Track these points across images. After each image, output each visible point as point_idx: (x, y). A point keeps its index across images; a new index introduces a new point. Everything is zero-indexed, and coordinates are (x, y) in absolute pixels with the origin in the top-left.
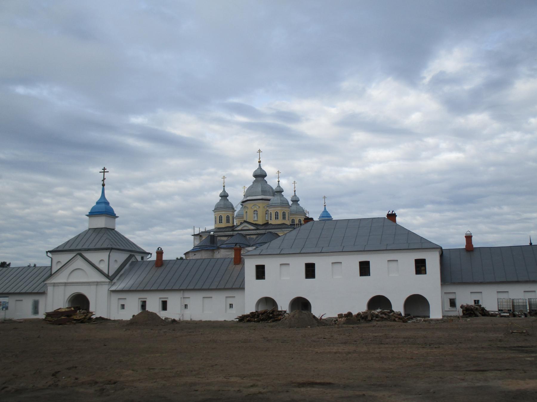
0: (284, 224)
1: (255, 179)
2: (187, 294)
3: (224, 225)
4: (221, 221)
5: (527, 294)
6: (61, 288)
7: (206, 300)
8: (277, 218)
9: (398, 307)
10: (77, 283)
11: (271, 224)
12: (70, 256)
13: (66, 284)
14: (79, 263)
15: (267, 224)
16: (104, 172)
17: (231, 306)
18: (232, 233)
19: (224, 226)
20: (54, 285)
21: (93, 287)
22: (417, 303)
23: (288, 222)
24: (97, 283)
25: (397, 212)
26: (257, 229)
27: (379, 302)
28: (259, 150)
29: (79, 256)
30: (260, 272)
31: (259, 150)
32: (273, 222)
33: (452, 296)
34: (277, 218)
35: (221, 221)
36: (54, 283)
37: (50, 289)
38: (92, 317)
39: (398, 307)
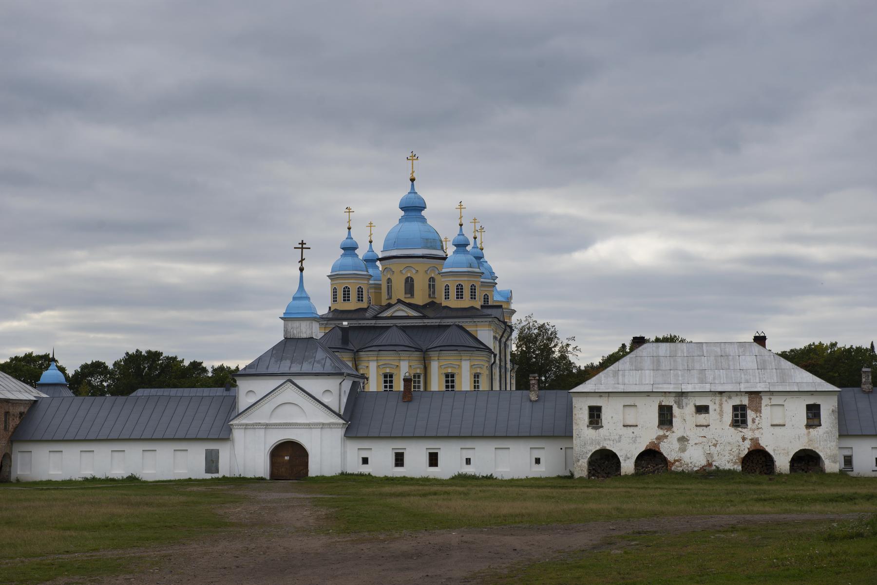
0: (472, 308)
1: (403, 213)
2: (469, 444)
3: (353, 305)
4: (346, 297)
5: (464, 451)
6: (261, 432)
7: (147, 454)
8: (460, 295)
9: (782, 463)
10: (280, 424)
11: (446, 307)
13: (267, 426)
14: (289, 394)
15: (432, 305)
16: (302, 248)
17: (538, 461)
18: (374, 322)
19: (353, 308)
20: (246, 426)
21: (316, 432)
22: (806, 460)
23: (478, 304)
24: (323, 426)
27: (758, 459)
29: (289, 384)
32: (453, 303)
33: (847, 453)
34: (460, 295)
35: (346, 297)
36: (247, 425)
37: (237, 434)
39: (782, 463)
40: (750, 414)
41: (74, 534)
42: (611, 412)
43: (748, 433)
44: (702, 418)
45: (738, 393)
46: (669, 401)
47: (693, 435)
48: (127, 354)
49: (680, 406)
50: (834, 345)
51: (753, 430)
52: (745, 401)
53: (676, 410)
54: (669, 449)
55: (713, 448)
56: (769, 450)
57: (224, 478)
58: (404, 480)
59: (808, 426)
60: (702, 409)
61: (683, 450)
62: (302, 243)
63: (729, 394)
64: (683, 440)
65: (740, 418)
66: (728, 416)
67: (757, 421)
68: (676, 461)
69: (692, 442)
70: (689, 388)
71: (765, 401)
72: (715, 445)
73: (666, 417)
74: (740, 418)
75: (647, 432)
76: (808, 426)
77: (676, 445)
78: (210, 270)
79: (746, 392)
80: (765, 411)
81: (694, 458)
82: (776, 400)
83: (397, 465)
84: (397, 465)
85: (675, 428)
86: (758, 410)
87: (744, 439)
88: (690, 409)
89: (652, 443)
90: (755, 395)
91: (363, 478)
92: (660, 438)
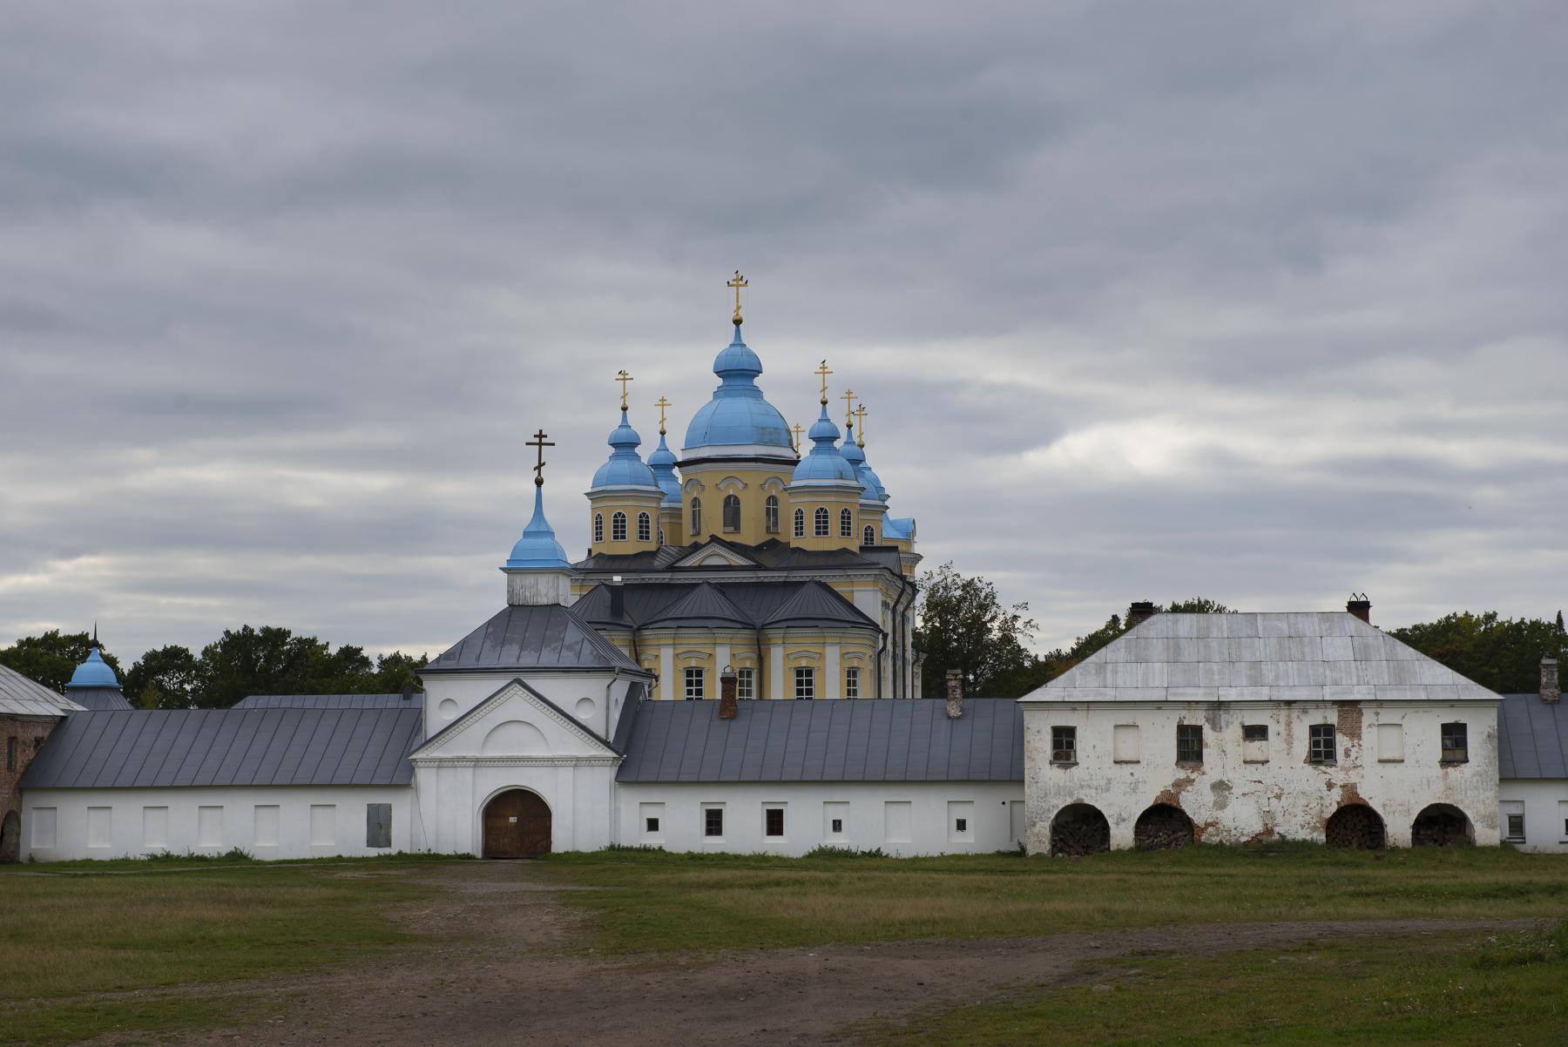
0: (844, 551)
1: (720, 381)
2: (838, 794)
3: (631, 545)
4: (619, 532)
6: (467, 774)
8: (822, 529)
9: (1399, 829)
10: (501, 760)
11: (798, 549)
12: (484, 687)
13: (477, 762)
14: (517, 704)
16: (540, 444)
17: (961, 825)
18: (668, 575)
19: (631, 552)
20: (440, 763)
21: (566, 774)
22: (1441, 824)
23: (854, 544)
24: (577, 762)
26: (758, 567)
27: (1355, 822)
29: (517, 687)
30: (1064, 741)
32: (810, 542)
33: (1515, 810)
34: (822, 529)
35: (619, 532)
36: (441, 760)
37: (424, 777)
38: (1518, 846)
39: (1399, 829)
40: (1342, 742)
41: (132, 955)
42: (1092, 737)
43: (1336, 774)
44: (1255, 749)
45: (1320, 704)
46: (1196, 718)
47: (1240, 778)
48: (227, 633)
49: (1216, 727)
50: (1490, 617)
51: (1346, 770)
52: (1332, 717)
53: (1208, 734)
54: (1197, 804)
55: (1274, 801)
56: (1375, 805)
57: (401, 855)
58: (722, 860)
59: (1445, 763)
60: (1255, 733)
61: (1221, 805)
63: (1304, 705)
64: (1220, 787)
65: (1322, 748)
66: (1302, 745)
67: (1353, 754)
68: (1208, 825)
69: (1236, 791)
70: (1231, 695)
71: (1368, 717)
72: (1278, 797)
73: (1190, 746)
74: (1322, 748)
75: (1157, 773)
76: (1445, 763)
77: (1209, 797)
78: (376, 483)
79: (1335, 702)
80: (1369, 735)
81: (1240, 819)
82: (1388, 716)
83: (709, 832)
84: (709, 832)
85: (1206, 767)
86: (1355, 734)
87: (1330, 786)
88: (1233, 732)
89: (1165, 793)
90: (1350, 708)
91: (649, 855)
92: (1180, 785)
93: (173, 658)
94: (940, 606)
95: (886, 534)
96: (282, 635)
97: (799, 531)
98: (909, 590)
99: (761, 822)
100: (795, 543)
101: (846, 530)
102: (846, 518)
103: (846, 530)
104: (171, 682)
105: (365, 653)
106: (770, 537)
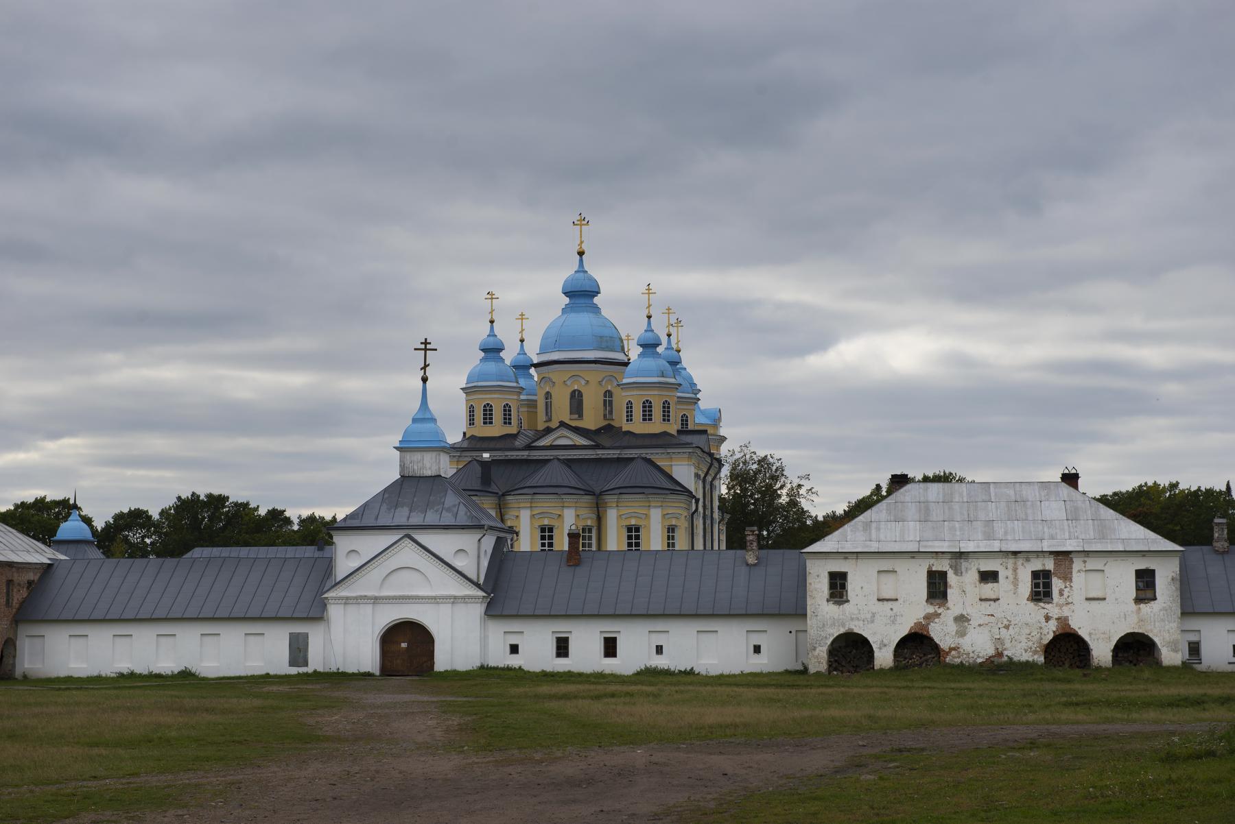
0: (665, 434)
2: (660, 625)
3: (497, 429)
4: (488, 419)
5: (654, 636)
6: (368, 609)
7: (206, 639)
8: (648, 416)
9: (1102, 652)
10: (395, 598)
11: (628, 432)
12: (381, 541)
13: (376, 600)
14: (408, 554)
17: (757, 649)
18: (526, 453)
19: (497, 434)
20: (347, 601)
21: (446, 609)
22: (1135, 648)
23: (673, 428)
24: (454, 600)
25: (1132, 606)
26: (597, 446)
27: (1067, 647)
28: (669, 309)
31: (669, 309)
32: (638, 426)
33: (1193, 638)
34: (648, 416)
35: (488, 419)
36: (347, 598)
37: (334, 611)
39: (1102, 652)
40: (1057, 584)
41: (104, 752)
42: (860, 580)
43: (1053, 610)
44: (988, 589)
45: (1040, 554)
46: (942, 565)
47: (977, 612)
48: (179, 498)
49: (957, 572)
51: (1060, 606)
52: (1049, 565)
53: (952, 578)
54: (943, 633)
55: (1004, 631)
56: (1083, 634)
57: (316, 673)
58: (569, 677)
59: (1138, 600)
60: (989, 577)
61: (961, 633)
62: (426, 343)
63: (1027, 555)
64: (961, 619)
65: (1041, 589)
66: (1026, 586)
67: (1066, 594)
68: (951, 649)
69: (974, 623)
70: (970, 547)
71: (1077, 564)
72: (1007, 627)
73: (937, 587)
74: (1041, 589)
75: (911, 608)
76: (1138, 600)
77: (952, 627)
80: (1078, 578)
81: (977, 645)
82: (1093, 563)
83: (559, 655)
84: (559, 655)
85: (950, 604)
86: (1067, 577)
87: (1047, 618)
88: (971, 576)
89: (918, 624)
90: (1063, 557)
91: (511, 673)
92: (929, 618)
93: (136, 518)
94: (740, 477)
95: (698, 420)
96: (222, 499)
97: (630, 418)
98: (716, 464)
99: (599, 647)
100: (626, 427)
101: (666, 417)
102: (666, 407)
103: (666, 417)
104: (134, 536)
105: (287, 514)
106: (607, 423)
